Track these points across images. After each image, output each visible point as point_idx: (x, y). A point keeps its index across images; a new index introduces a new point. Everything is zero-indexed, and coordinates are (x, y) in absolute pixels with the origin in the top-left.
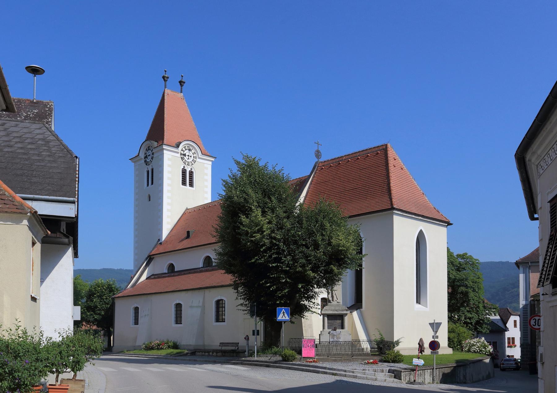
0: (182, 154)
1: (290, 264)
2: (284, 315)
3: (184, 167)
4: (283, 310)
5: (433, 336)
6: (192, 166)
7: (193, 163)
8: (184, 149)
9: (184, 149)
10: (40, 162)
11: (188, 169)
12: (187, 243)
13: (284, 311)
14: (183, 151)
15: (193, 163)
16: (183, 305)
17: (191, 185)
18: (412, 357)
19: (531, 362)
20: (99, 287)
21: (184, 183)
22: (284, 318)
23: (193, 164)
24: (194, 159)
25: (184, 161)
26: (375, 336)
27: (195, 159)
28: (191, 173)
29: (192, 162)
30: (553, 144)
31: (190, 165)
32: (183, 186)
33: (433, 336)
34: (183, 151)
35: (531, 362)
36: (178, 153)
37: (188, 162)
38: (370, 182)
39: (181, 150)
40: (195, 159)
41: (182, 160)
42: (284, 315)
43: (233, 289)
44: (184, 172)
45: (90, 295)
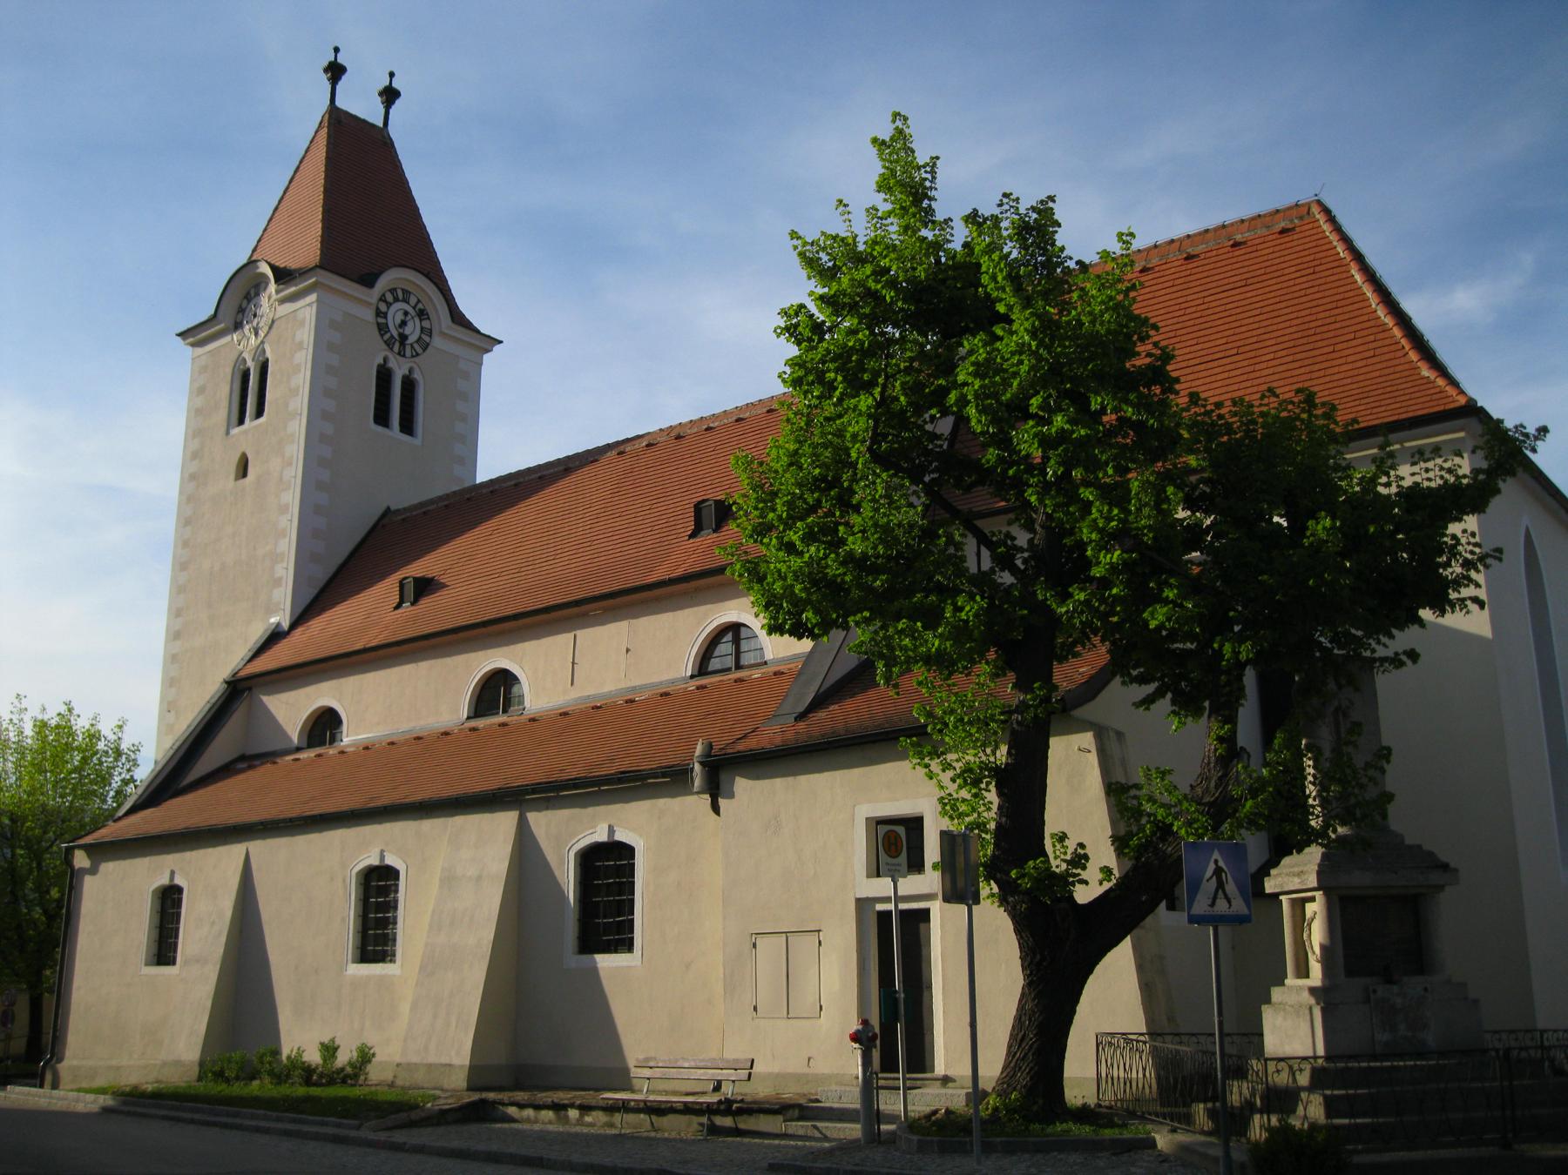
1: (941, 635)
2: (1221, 885)
3: (385, 359)
4: (1216, 855)
5: (623, 943)
6: (413, 359)
7: (419, 350)
8: (390, 298)
9: (390, 298)
11: (399, 369)
13: (1221, 864)
14: (385, 301)
15: (419, 350)
17: (407, 426)
20: (845, 295)
21: (382, 417)
23: (417, 355)
24: (423, 336)
25: (387, 336)
27: (427, 338)
28: (409, 385)
29: (416, 346)
30: (385, 651)
31: (408, 353)
32: (380, 429)
33: (623, 943)
34: (385, 301)
36: (368, 304)
38: (1160, 286)
39: (380, 300)
40: (427, 338)
41: (382, 335)
42: (1221, 885)
44: (384, 376)
45: (880, 187)
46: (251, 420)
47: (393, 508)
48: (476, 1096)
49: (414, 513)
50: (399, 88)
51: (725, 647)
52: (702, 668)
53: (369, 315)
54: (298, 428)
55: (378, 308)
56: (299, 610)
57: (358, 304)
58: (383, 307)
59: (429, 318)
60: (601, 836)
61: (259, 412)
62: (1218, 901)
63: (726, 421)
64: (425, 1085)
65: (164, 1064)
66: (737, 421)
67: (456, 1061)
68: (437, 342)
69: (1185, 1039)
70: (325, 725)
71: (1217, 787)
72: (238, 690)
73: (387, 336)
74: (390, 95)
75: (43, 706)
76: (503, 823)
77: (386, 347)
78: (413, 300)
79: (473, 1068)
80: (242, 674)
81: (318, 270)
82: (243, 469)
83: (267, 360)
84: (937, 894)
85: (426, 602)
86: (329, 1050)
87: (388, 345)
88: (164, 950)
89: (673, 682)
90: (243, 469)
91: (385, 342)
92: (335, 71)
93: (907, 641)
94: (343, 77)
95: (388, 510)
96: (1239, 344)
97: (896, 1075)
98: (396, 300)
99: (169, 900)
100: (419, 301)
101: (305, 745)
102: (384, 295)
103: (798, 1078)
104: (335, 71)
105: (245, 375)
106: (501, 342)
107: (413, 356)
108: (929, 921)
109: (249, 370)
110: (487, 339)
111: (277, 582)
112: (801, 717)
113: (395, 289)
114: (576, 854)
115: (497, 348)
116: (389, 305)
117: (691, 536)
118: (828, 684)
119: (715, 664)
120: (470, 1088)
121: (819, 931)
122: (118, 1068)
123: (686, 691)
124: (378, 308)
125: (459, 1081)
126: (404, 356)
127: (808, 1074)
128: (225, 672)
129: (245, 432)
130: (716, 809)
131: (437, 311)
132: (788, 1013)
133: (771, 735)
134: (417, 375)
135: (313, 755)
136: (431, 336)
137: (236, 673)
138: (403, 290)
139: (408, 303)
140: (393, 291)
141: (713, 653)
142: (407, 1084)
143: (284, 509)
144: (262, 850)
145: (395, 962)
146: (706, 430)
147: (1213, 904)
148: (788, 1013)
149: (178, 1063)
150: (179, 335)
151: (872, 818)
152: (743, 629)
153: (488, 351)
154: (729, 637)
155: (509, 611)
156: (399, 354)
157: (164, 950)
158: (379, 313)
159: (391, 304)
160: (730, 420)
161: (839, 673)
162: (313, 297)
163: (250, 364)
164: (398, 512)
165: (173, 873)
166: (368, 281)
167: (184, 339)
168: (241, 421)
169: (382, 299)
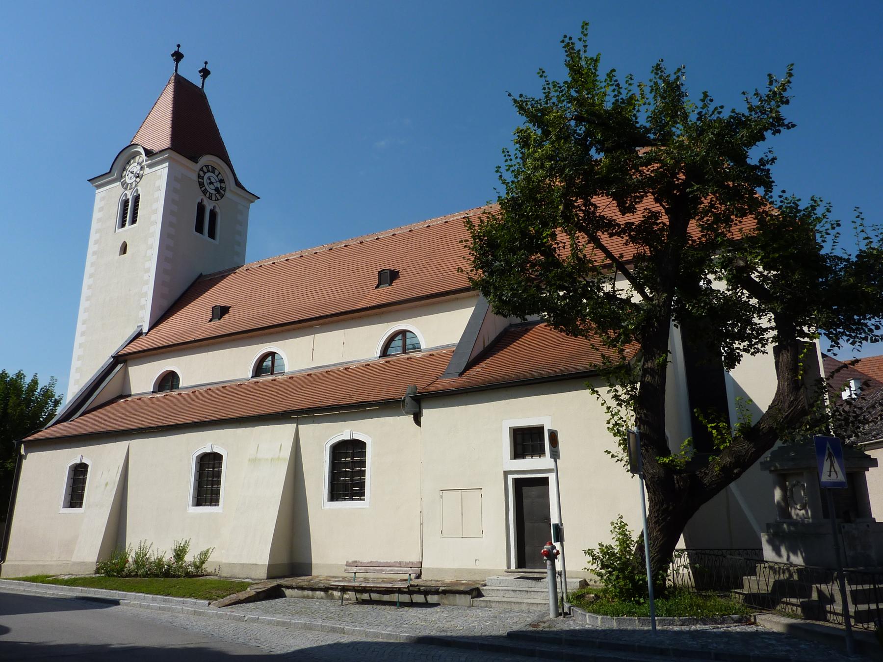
0: (201, 176)
3: (202, 200)
6: (216, 202)
7: (219, 198)
10: (437, 353)
11: (209, 206)
12: (386, 294)
14: (203, 171)
16: (195, 231)
17: (212, 234)
18: (715, 279)
19: (694, 184)
21: (199, 228)
22: (834, 477)
23: (218, 200)
26: (844, 252)
28: (213, 214)
30: (221, 339)
31: (213, 199)
34: (203, 171)
35: (694, 184)
37: (210, 193)
39: (200, 170)
41: (201, 188)
43: (612, 541)
44: (201, 208)
46: (129, 225)
47: (203, 274)
48: (274, 583)
49: (216, 277)
50: (209, 70)
51: (398, 342)
52: (384, 353)
53: (195, 177)
54: (157, 229)
55: (199, 174)
56: (151, 326)
57: (191, 170)
58: (202, 174)
59: (224, 182)
60: (346, 437)
61: (134, 221)
62: (832, 473)
63: (387, 235)
64: (241, 576)
65: (74, 563)
66: (393, 235)
67: (260, 562)
68: (228, 194)
69: (741, 551)
70: (168, 381)
71: (789, 407)
72: (121, 360)
73: (203, 188)
74: (205, 73)
75: (260, 198)
76: (284, 432)
77: (203, 194)
78: (217, 173)
79: (270, 566)
80: (122, 353)
81: (169, 151)
82: (124, 249)
83: (139, 195)
84: (553, 469)
85: (226, 317)
86: (180, 554)
87: (204, 193)
88: (75, 497)
89: (296, 372)
90: (124, 249)
91: (202, 191)
92: (178, 56)
93: (635, 319)
94: (182, 60)
95: (201, 275)
96: (443, 272)
97: (545, 570)
98: (208, 171)
99: (79, 472)
100: (220, 173)
101: (157, 391)
102: (202, 168)
103: (469, 571)
104: (178, 56)
105: (126, 203)
106: (259, 198)
107: (216, 200)
108: (548, 485)
109: (128, 199)
110: (252, 196)
111: (143, 307)
112: (461, 374)
113: (208, 166)
114: (330, 446)
115: (257, 201)
116: (205, 173)
117: (376, 288)
118: (472, 358)
119: (391, 351)
120: (270, 577)
121: (481, 489)
122: (44, 566)
123: (379, 364)
124: (199, 174)
125: (262, 574)
126: (211, 199)
127: (475, 569)
128: (113, 351)
129: (126, 231)
130: (418, 421)
131: (228, 177)
132: (462, 535)
133: (445, 383)
134: (217, 210)
135: (163, 395)
136: (225, 191)
137: (118, 353)
138: (212, 166)
139: (214, 173)
140: (207, 166)
141: (390, 346)
142: (229, 575)
143: (148, 271)
144: (136, 444)
145: (218, 505)
146: (377, 239)
147: (830, 476)
148: (462, 535)
149: (83, 564)
150: (89, 181)
151: (512, 427)
152: (407, 333)
153: (252, 202)
154: (400, 337)
155: (276, 323)
156: (209, 198)
157: (75, 497)
158: (199, 176)
159: (206, 173)
160: (389, 235)
161: (475, 354)
162: (167, 164)
163: (130, 197)
164: (206, 276)
165: (82, 456)
166: (195, 161)
167: (92, 184)
168: (123, 225)
169: (201, 169)
